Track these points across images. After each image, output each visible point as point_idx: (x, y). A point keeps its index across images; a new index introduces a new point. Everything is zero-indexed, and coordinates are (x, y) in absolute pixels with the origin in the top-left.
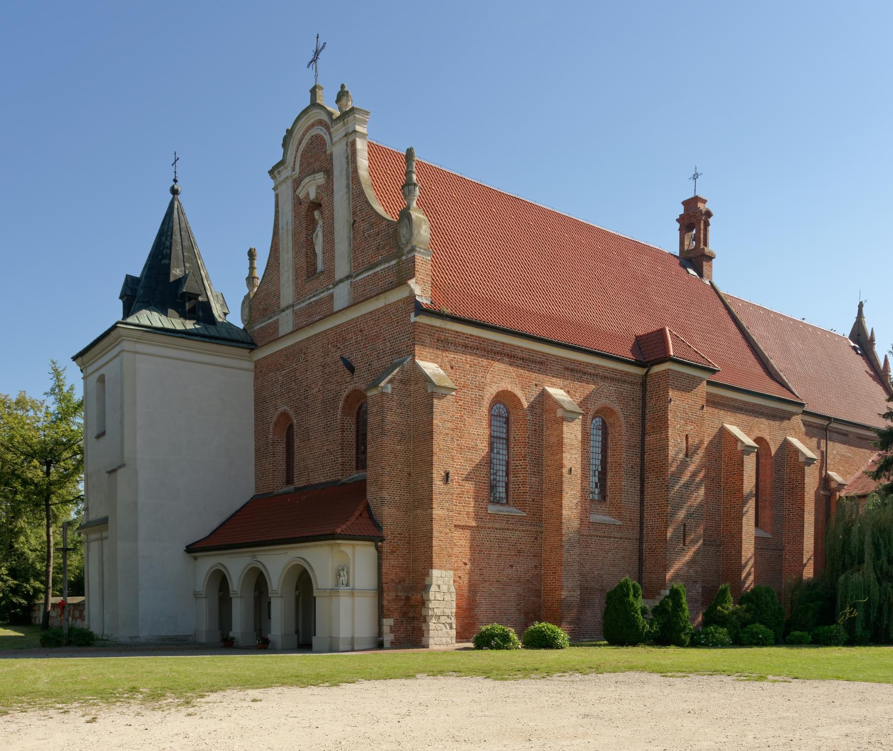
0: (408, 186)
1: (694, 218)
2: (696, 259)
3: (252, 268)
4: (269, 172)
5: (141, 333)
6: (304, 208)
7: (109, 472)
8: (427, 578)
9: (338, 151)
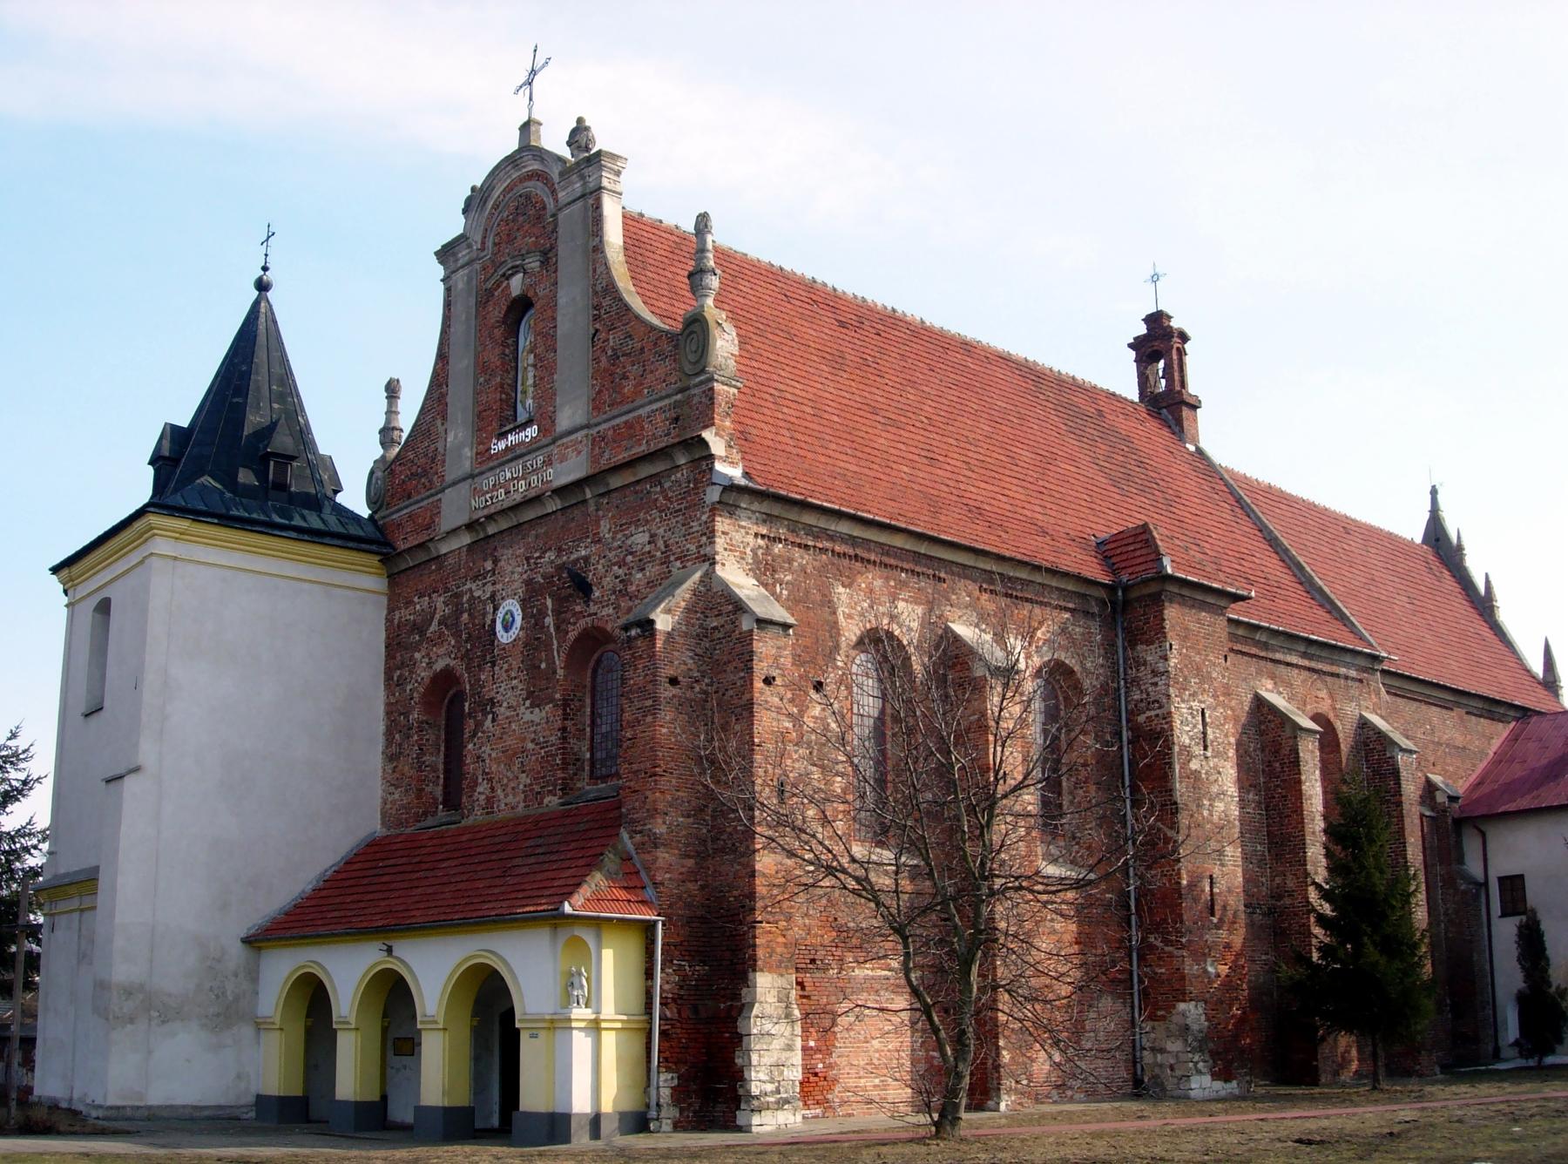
0: (696, 276)
1: (1158, 343)
2: (1169, 405)
3: (391, 412)
6: (496, 312)
7: (108, 781)
8: (744, 991)
9: (569, 220)
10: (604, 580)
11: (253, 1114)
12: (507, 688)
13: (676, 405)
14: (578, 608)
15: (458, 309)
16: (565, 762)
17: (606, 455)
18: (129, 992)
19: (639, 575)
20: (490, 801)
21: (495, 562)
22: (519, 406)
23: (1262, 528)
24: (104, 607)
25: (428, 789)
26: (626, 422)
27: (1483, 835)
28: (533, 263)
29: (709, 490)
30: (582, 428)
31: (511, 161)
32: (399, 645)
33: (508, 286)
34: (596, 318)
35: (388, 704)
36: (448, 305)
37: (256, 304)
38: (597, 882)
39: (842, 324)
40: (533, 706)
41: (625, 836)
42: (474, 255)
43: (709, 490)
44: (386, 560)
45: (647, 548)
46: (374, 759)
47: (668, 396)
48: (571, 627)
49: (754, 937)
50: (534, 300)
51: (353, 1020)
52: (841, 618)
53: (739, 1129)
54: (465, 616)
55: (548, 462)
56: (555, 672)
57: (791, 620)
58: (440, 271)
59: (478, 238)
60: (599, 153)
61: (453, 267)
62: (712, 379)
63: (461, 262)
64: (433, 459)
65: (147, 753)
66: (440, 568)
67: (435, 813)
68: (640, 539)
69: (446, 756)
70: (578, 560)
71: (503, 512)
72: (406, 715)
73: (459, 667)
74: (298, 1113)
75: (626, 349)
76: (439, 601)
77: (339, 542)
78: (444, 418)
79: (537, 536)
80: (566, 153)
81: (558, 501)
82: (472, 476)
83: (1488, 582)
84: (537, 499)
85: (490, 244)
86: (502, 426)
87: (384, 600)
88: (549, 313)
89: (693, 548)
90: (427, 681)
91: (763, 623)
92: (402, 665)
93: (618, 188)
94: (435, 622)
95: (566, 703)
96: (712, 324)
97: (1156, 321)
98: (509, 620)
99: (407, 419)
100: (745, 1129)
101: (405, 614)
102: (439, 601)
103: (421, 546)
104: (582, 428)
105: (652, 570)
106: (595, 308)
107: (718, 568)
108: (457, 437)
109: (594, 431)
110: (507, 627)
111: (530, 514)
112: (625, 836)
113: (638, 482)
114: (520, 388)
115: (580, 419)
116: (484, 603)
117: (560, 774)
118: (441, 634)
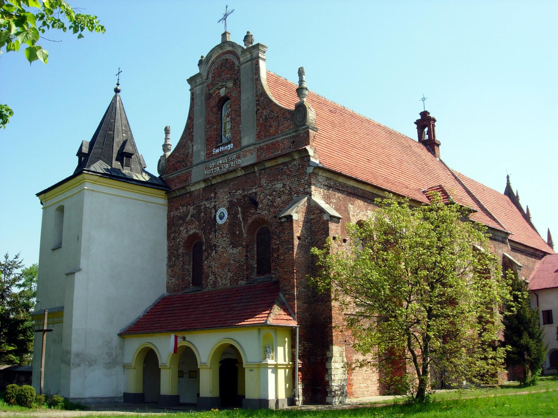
1: (425, 122)
5: (98, 177)
6: (213, 103)
7: (67, 275)
8: (328, 353)
9: (245, 69)
10: (264, 200)
11: (122, 400)
12: (222, 241)
13: (293, 137)
14: (252, 211)
15: (197, 100)
16: (247, 268)
17: (264, 155)
18: (78, 355)
19: (279, 199)
20: (215, 283)
21: (216, 194)
22: (223, 137)
23: (465, 188)
24: (61, 209)
25: (186, 278)
26: (272, 143)
27: (537, 296)
28: (230, 84)
29: (308, 168)
30: (253, 145)
31: (219, 47)
32: (173, 225)
33: (219, 93)
34: (257, 105)
35: (169, 247)
36: (192, 99)
37: (115, 97)
38: (277, 310)
39: (331, 111)
40: (233, 247)
41: (281, 295)
42: (204, 81)
43: (308, 168)
44: (168, 193)
45: (282, 189)
46: (163, 267)
47: (290, 133)
48: (249, 218)
49: (332, 333)
50: (230, 97)
51: (168, 364)
52: (351, 216)
53: (328, 404)
54: (203, 214)
55: (238, 157)
56: (243, 235)
57: (340, 217)
58: (189, 87)
59: (205, 75)
60: (258, 45)
61: (194, 85)
62: (308, 128)
63: (198, 83)
64: (187, 156)
65: (83, 263)
66: (190, 196)
67: (189, 287)
68: (279, 186)
69: (193, 266)
70: (252, 193)
71: (220, 175)
72: (177, 251)
73: (201, 233)
74: (130, 401)
75: (272, 116)
76: (191, 209)
77: (151, 186)
78: (192, 140)
79: (233, 185)
80: (242, 44)
81: (243, 172)
82: (205, 162)
83: (528, 209)
84: (235, 171)
85: (210, 76)
86: (217, 144)
87: (166, 208)
88: (237, 102)
89: (302, 189)
90: (186, 238)
91: (332, 217)
92: (175, 232)
93: (264, 57)
94: (189, 216)
95: (247, 246)
96: (307, 108)
97: (424, 114)
98: (222, 216)
99: (174, 142)
100: (330, 403)
101: (174, 213)
102: (191, 209)
103: (183, 188)
104: (253, 145)
105: (284, 198)
106: (257, 101)
107: (313, 197)
108: (198, 149)
109: (258, 146)
110: (221, 218)
111: (231, 176)
112: (281, 295)
113: (277, 165)
114: (223, 130)
115: (252, 141)
116: (211, 209)
117: (246, 273)
118: (192, 221)
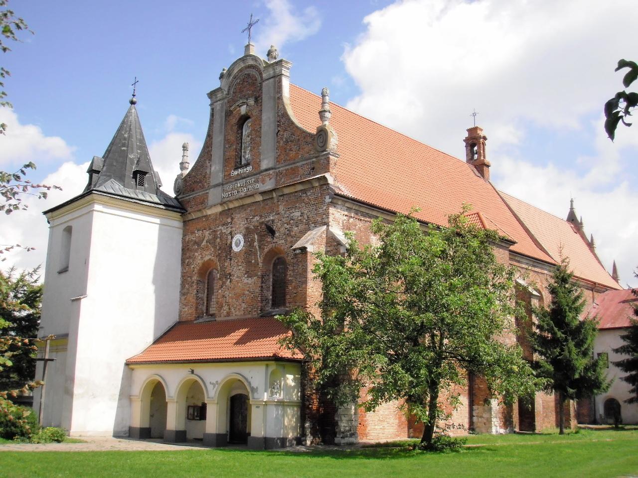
1: (474, 141)
4: (208, 94)
